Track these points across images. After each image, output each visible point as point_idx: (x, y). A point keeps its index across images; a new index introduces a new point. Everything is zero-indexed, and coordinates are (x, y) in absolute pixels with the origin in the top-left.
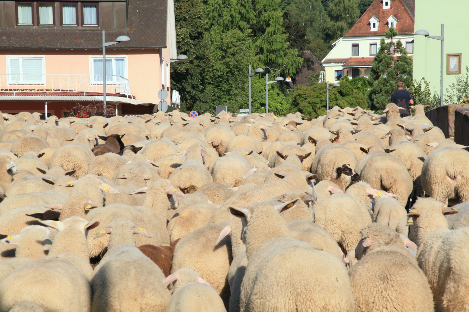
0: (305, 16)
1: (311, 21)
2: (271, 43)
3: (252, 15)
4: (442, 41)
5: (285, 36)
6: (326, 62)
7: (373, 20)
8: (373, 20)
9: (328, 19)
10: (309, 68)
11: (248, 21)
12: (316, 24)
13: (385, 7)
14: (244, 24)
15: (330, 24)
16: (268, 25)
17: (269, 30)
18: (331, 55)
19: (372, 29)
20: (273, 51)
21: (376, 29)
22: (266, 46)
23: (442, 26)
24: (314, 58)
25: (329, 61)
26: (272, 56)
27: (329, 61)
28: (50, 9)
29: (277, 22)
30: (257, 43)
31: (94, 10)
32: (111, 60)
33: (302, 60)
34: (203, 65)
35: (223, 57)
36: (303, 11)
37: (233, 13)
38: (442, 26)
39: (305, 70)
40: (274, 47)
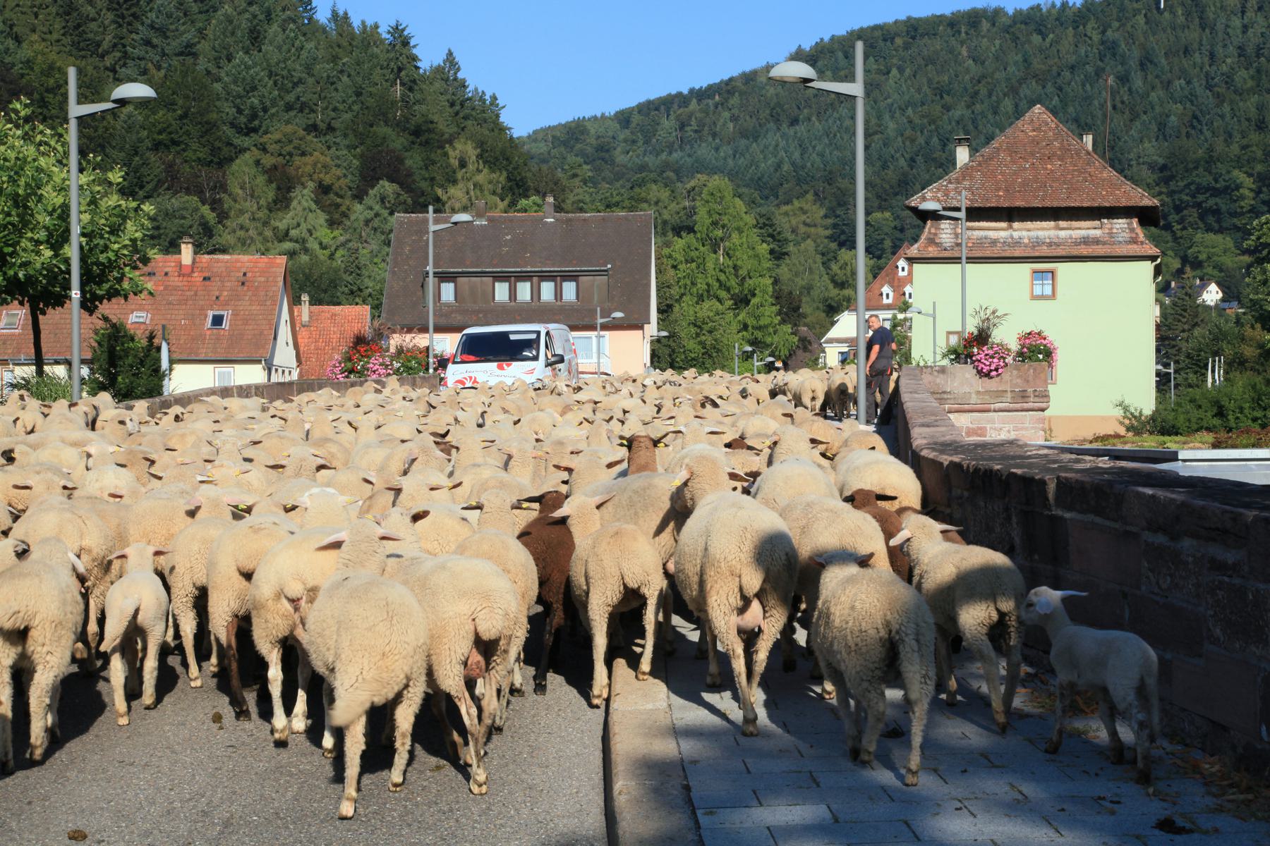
0: (800, 282)
1: (809, 288)
2: (757, 318)
3: (733, 282)
4: (934, 318)
5: (775, 308)
6: (826, 342)
7: (886, 289)
8: (886, 289)
9: (831, 286)
10: (805, 349)
11: (728, 290)
12: (815, 293)
13: (901, 274)
14: (723, 294)
15: (834, 292)
16: (754, 295)
17: (754, 301)
18: (834, 333)
19: (885, 301)
20: (760, 328)
21: (890, 301)
22: (751, 322)
23: (934, 303)
24: (811, 337)
25: (831, 341)
26: (759, 334)
27: (831, 341)
28: (528, 285)
29: (764, 292)
30: (740, 318)
31: (573, 285)
32: (590, 338)
33: (796, 339)
34: (673, 344)
35: (698, 335)
36: (797, 275)
37: (710, 280)
38: (934, 303)
39: (800, 352)
40: (761, 323)
